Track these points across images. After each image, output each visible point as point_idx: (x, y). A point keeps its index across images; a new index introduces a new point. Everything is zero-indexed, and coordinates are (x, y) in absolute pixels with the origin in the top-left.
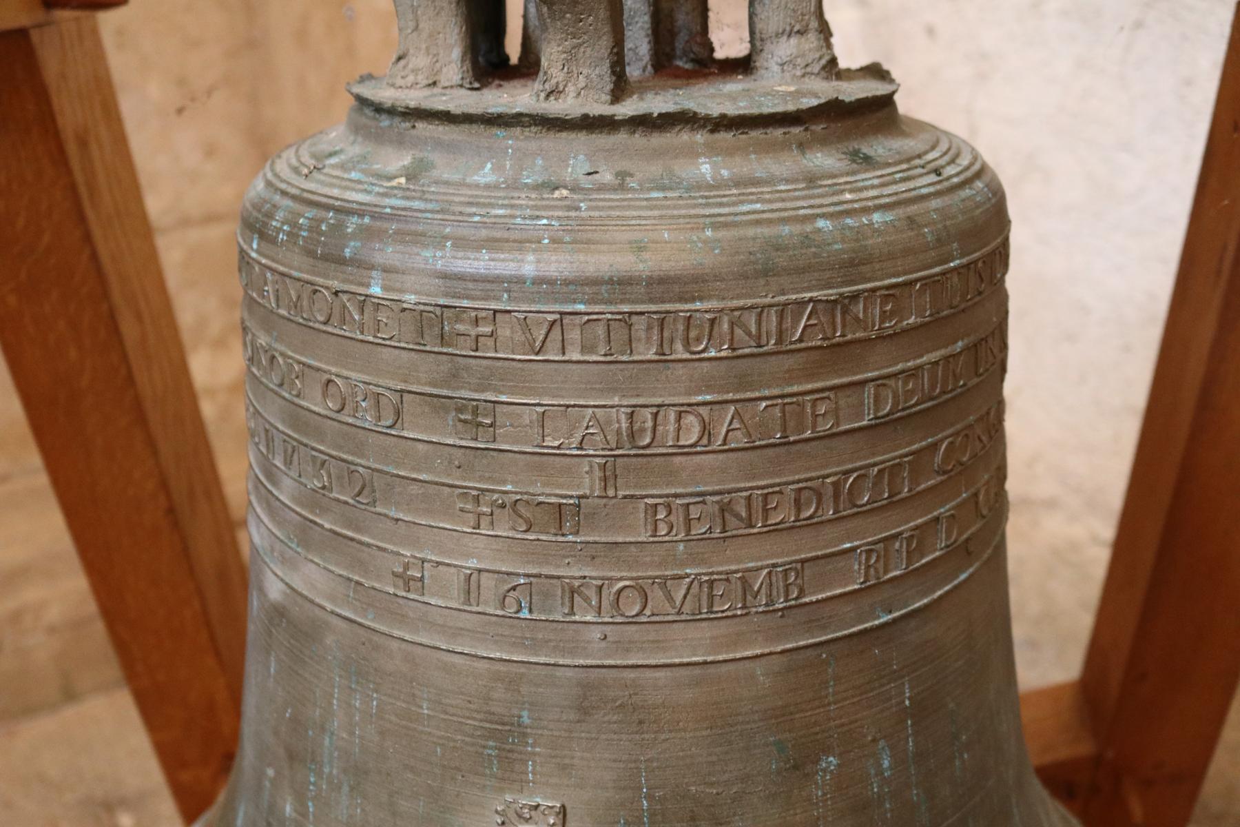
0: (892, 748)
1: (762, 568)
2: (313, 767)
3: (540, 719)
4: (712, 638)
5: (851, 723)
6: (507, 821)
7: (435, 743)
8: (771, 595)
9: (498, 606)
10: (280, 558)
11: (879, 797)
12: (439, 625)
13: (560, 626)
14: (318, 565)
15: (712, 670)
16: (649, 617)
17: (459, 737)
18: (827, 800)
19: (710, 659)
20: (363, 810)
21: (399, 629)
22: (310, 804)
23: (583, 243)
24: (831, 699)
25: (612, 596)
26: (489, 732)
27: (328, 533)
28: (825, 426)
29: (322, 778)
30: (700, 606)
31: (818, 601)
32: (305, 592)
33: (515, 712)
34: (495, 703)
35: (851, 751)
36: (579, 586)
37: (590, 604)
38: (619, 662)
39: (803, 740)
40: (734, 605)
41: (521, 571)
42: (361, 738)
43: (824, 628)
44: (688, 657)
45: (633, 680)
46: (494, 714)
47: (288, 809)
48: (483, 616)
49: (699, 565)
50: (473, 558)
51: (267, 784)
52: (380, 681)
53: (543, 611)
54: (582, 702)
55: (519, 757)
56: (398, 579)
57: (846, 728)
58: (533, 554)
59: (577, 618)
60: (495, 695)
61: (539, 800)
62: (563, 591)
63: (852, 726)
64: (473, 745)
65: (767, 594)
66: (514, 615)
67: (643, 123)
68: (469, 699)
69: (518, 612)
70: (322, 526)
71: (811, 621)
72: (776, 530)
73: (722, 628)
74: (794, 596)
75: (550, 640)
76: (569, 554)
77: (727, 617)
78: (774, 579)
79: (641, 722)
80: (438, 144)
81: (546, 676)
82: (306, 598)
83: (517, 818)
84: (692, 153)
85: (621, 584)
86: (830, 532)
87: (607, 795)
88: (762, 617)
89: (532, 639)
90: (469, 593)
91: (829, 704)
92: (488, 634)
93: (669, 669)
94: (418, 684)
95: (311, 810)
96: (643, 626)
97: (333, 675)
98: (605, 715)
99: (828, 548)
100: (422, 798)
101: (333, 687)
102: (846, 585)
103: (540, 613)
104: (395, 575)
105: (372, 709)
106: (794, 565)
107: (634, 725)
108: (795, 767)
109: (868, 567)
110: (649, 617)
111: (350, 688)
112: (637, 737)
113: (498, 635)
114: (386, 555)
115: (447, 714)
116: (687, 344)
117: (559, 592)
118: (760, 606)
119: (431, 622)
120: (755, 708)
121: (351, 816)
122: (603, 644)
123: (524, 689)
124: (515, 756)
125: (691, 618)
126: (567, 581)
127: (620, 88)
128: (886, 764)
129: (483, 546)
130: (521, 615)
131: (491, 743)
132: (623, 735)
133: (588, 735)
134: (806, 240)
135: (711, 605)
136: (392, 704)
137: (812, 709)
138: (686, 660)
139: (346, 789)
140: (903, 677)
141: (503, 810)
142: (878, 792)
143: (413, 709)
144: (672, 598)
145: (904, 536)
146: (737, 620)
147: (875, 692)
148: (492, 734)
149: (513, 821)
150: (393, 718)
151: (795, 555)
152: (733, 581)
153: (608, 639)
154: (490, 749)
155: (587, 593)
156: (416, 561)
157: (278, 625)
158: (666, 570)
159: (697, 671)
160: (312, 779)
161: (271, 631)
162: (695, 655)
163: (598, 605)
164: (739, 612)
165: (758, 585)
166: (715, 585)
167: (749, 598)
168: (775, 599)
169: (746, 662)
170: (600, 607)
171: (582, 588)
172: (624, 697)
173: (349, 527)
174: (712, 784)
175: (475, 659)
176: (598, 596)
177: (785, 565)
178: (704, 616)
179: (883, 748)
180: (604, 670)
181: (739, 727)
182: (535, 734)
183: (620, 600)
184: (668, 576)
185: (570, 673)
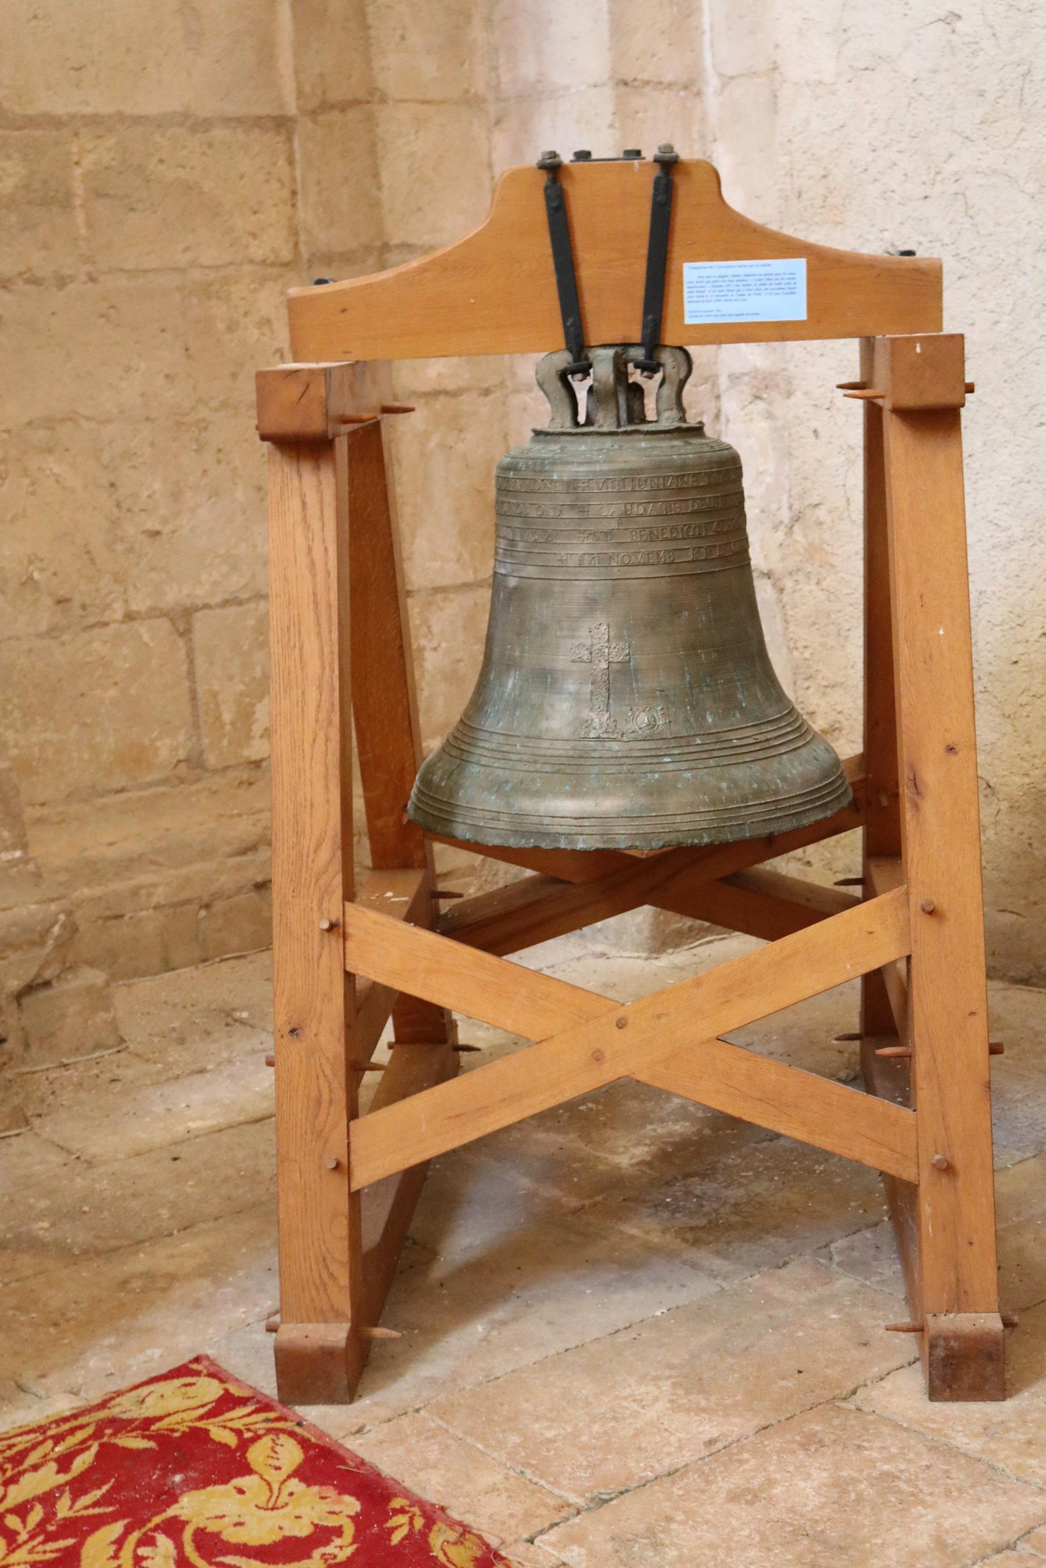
23: (611, 462)
28: (678, 511)
67: (626, 433)
72: (666, 539)
80: (568, 442)
84: (640, 441)
86: (681, 542)
116: (640, 486)
127: (619, 425)
134: (670, 461)
159: (642, 581)
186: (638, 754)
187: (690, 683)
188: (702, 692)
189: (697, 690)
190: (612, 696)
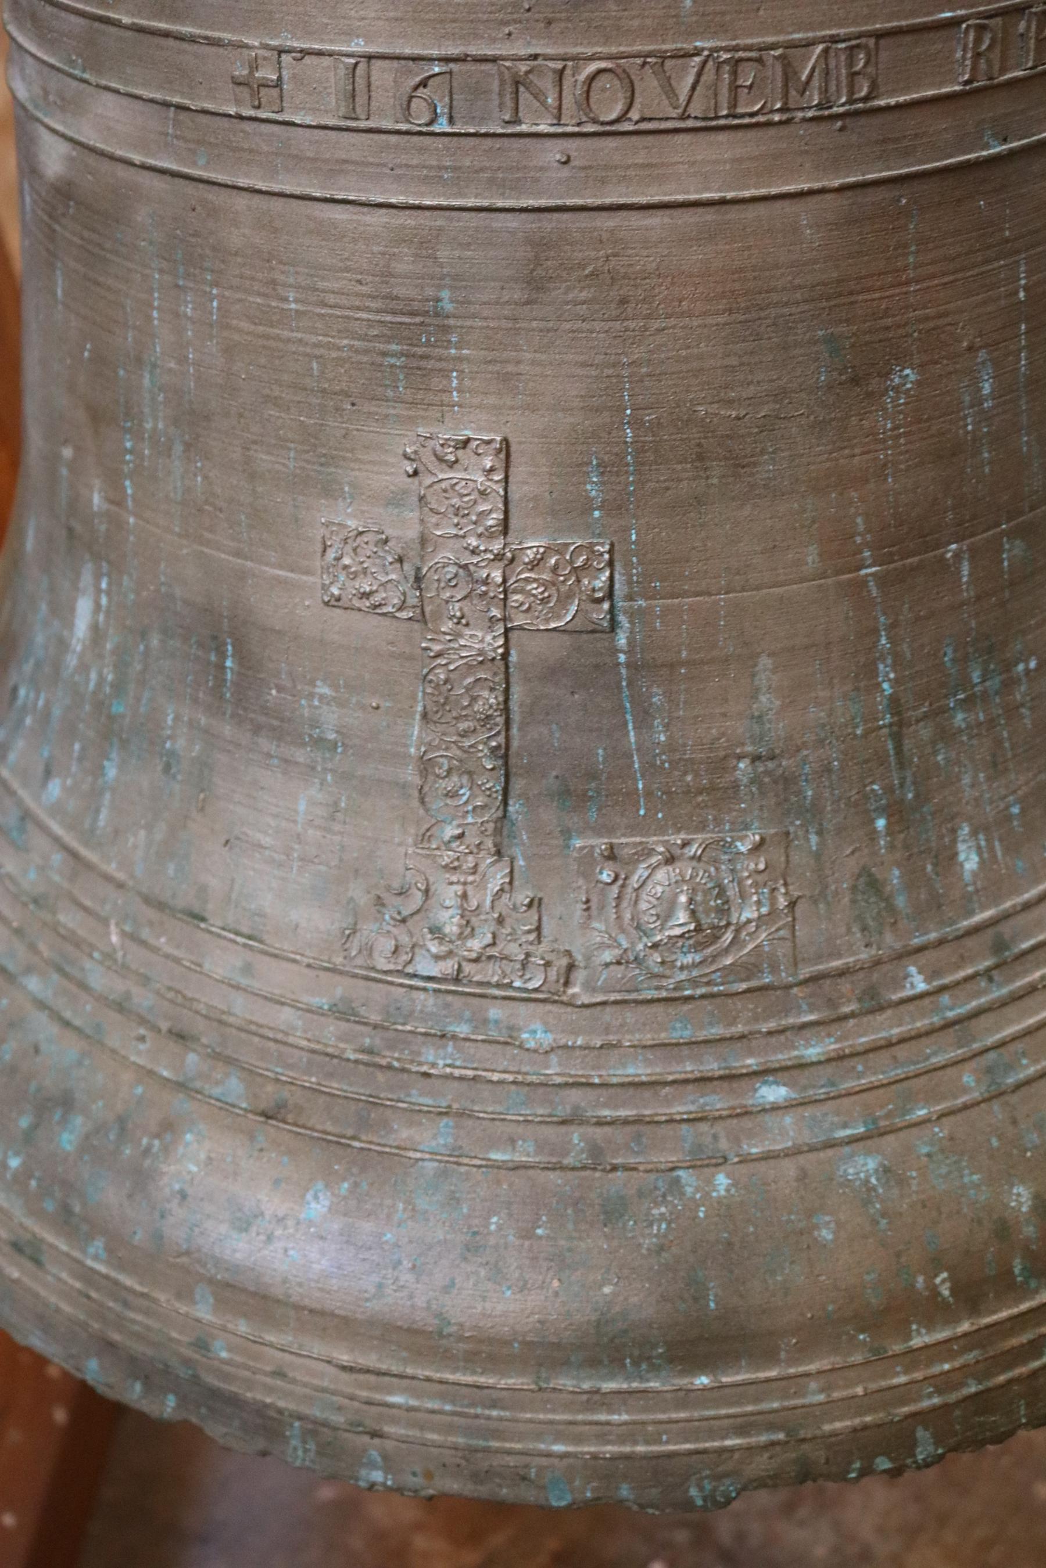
0: (996, 364)
1: (810, 44)
2: (129, 424)
3: (470, 303)
4: (734, 160)
5: (940, 316)
6: (421, 468)
7: (307, 355)
8: (826, 91)
9: (399, 115)
10: (59, 102)
11: (974, 440)
12: (308, 158)
13: (498, 143)
14: (117, 92)
15: (733, 214)
16: (637, 123)
17: (345, 342)
18: (899, 436)
19: (730, 195)
20: (205, 477)
21: (247, 175)
22: (128, 483)
24: (911, 274)
25: (579, 87)
26: (391, 329)
27: (129, 34)
29: (143, 439)
30: (716, 103)
31: (899, 106)
32: (100, 145)
33: (430, 292)
34: (400, 280)
35: (936, 363)
36: (527, 73)
37: (544, 104)
38: (590, 201)
39: (867, 338)
40: (769, 105)
41: (435, 52)
42: (197, 364)
43: (907, 154)
44: (697, 192)
45: (612, 232)
46: (397, 298)
47: (96, 499)
48: (376, 136)
49: (715, 35)
50: (358, 37)
51: (64, 471)
52: (223, 266)
53: (471, 120)
54: (533, 270)
55: (439, 365)
56: (241, 88)
57: (931, 324)
58: (454, 21)
59: (524, 128)
60: (400, 267)
61: (469, 433)
62: (502, 82)
63: (941, 322)
64: (366, 352)
65: (820, 88)
66: (424, 129)
68: (359, 277)
69: (430, 123)
70: (117, 24)
71: (884, 141)
73: (748, 144)
74: (863, 94)
75: (482, 170)
76: (509, 17)
77: (757, 125)
78: (832, 63)
79: (623, 301)
81: (477, 229)
82: (102, 154)
83: (437, 463)
85: (593, 67)
87: (572, 420)
88: (814, 128)
89: (455, 169)
90: (354, 97)
91: (908, 283)
92: (384, 165)
93: (668, 212)
94: (281, 262)
95: (129, 491)
96: (625, 140)
97: (147, 271)
98: (568, 289)
99: (918, 17)
100: (292, 445)
101: (151, 291)
102: (941, 85)
103: (466, 123)
104: (238, 83)
105: (211, 314)
106: (863, 40)
107: (613, 306)
108: (855, 381)
109: (977, 55)
110: (637, 123)
111: (177, 286)
112: (617, 325)
113: (400, 166)
114: (221, 50)
115: (326, 305)
117: (495, 86)
118: (810, 108)
119: (297, 156)
120: (797, 281)
121: (188, 490)
122: (565, 172)
123: (444, 254)
124: (430, 364)
125: (703, 124)
126: (508, 64)
128: (987, 389)
129: (373, 15)
130: (436, 128)
131: (394, 347)
132: (595, 323)
133: (542, 325)
135: (734, 104)
136: (240, 300)
137: (881, 288)
138: (693, 197)
139: (178, 448)
140: (1018, 252)
141: (416, 452)
142: (973, 430)
143: (274, 304)
144: (673, 91)
145: (1034, 10)
146: (772, 132)
147: (976, 271)
148: (395, 332)
149: (431, 468)
150: (244, 325)
151: (866, 24)
152: (770, 62)
153: (573, 163)
154: (392, 356)
155: (539, 84)
156: (267, 54)
157: (64, 215)
158: (664, 42)
159: (709, 215)
160: (128, 445)
161: (54, 231)
162: (708, 189)
163: (557, 104)
164: (777, 118)
165: (807, 72)
166: (740, 69)
167: (793, 93)
168: (833, 98)
169: (786, 203)
170: (560, 108)
171: (531, 76)
172: (597, 259)
173: (158, 16)
174: (730, 403)
175: (366, 209)
176: (557, 89)
177: (849, 39)
178: (722, 122)
179: (983, 363)
180: (566, 216)
181: (773, 312)
182: (462, 327)
183: (592, 94)
184: (666, 51)
185: (512, 222)
186: (637, 1070)
187: (895, 704)
188: (946, 735)
189: (925, 732)
190: (518, 785)
